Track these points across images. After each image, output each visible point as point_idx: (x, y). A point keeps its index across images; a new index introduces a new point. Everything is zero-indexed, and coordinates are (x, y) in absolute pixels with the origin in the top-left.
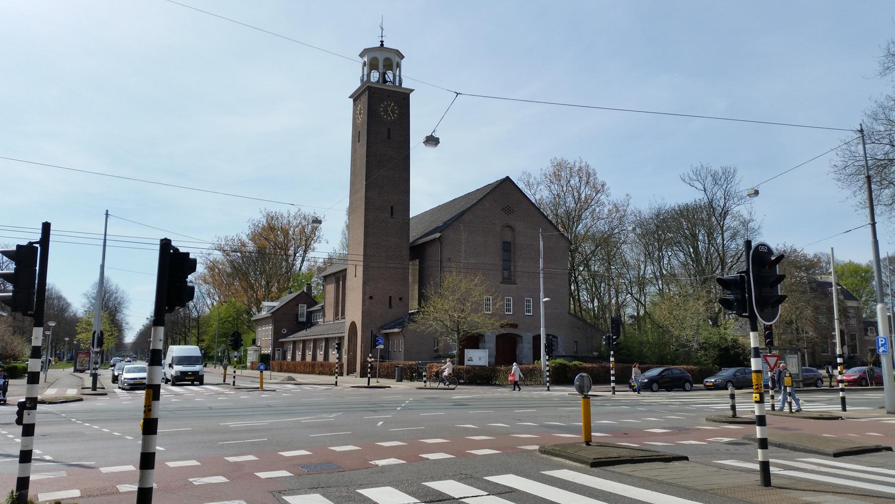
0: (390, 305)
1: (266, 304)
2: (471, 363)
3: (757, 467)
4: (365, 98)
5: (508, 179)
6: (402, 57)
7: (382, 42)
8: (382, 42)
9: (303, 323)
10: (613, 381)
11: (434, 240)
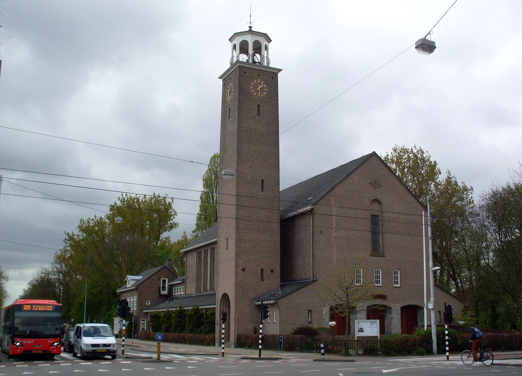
1: (130, 277)
6: (269, 40)
7: (250, 27)
8: (250, 27)
9: (164, 296)
10: (448, 351)
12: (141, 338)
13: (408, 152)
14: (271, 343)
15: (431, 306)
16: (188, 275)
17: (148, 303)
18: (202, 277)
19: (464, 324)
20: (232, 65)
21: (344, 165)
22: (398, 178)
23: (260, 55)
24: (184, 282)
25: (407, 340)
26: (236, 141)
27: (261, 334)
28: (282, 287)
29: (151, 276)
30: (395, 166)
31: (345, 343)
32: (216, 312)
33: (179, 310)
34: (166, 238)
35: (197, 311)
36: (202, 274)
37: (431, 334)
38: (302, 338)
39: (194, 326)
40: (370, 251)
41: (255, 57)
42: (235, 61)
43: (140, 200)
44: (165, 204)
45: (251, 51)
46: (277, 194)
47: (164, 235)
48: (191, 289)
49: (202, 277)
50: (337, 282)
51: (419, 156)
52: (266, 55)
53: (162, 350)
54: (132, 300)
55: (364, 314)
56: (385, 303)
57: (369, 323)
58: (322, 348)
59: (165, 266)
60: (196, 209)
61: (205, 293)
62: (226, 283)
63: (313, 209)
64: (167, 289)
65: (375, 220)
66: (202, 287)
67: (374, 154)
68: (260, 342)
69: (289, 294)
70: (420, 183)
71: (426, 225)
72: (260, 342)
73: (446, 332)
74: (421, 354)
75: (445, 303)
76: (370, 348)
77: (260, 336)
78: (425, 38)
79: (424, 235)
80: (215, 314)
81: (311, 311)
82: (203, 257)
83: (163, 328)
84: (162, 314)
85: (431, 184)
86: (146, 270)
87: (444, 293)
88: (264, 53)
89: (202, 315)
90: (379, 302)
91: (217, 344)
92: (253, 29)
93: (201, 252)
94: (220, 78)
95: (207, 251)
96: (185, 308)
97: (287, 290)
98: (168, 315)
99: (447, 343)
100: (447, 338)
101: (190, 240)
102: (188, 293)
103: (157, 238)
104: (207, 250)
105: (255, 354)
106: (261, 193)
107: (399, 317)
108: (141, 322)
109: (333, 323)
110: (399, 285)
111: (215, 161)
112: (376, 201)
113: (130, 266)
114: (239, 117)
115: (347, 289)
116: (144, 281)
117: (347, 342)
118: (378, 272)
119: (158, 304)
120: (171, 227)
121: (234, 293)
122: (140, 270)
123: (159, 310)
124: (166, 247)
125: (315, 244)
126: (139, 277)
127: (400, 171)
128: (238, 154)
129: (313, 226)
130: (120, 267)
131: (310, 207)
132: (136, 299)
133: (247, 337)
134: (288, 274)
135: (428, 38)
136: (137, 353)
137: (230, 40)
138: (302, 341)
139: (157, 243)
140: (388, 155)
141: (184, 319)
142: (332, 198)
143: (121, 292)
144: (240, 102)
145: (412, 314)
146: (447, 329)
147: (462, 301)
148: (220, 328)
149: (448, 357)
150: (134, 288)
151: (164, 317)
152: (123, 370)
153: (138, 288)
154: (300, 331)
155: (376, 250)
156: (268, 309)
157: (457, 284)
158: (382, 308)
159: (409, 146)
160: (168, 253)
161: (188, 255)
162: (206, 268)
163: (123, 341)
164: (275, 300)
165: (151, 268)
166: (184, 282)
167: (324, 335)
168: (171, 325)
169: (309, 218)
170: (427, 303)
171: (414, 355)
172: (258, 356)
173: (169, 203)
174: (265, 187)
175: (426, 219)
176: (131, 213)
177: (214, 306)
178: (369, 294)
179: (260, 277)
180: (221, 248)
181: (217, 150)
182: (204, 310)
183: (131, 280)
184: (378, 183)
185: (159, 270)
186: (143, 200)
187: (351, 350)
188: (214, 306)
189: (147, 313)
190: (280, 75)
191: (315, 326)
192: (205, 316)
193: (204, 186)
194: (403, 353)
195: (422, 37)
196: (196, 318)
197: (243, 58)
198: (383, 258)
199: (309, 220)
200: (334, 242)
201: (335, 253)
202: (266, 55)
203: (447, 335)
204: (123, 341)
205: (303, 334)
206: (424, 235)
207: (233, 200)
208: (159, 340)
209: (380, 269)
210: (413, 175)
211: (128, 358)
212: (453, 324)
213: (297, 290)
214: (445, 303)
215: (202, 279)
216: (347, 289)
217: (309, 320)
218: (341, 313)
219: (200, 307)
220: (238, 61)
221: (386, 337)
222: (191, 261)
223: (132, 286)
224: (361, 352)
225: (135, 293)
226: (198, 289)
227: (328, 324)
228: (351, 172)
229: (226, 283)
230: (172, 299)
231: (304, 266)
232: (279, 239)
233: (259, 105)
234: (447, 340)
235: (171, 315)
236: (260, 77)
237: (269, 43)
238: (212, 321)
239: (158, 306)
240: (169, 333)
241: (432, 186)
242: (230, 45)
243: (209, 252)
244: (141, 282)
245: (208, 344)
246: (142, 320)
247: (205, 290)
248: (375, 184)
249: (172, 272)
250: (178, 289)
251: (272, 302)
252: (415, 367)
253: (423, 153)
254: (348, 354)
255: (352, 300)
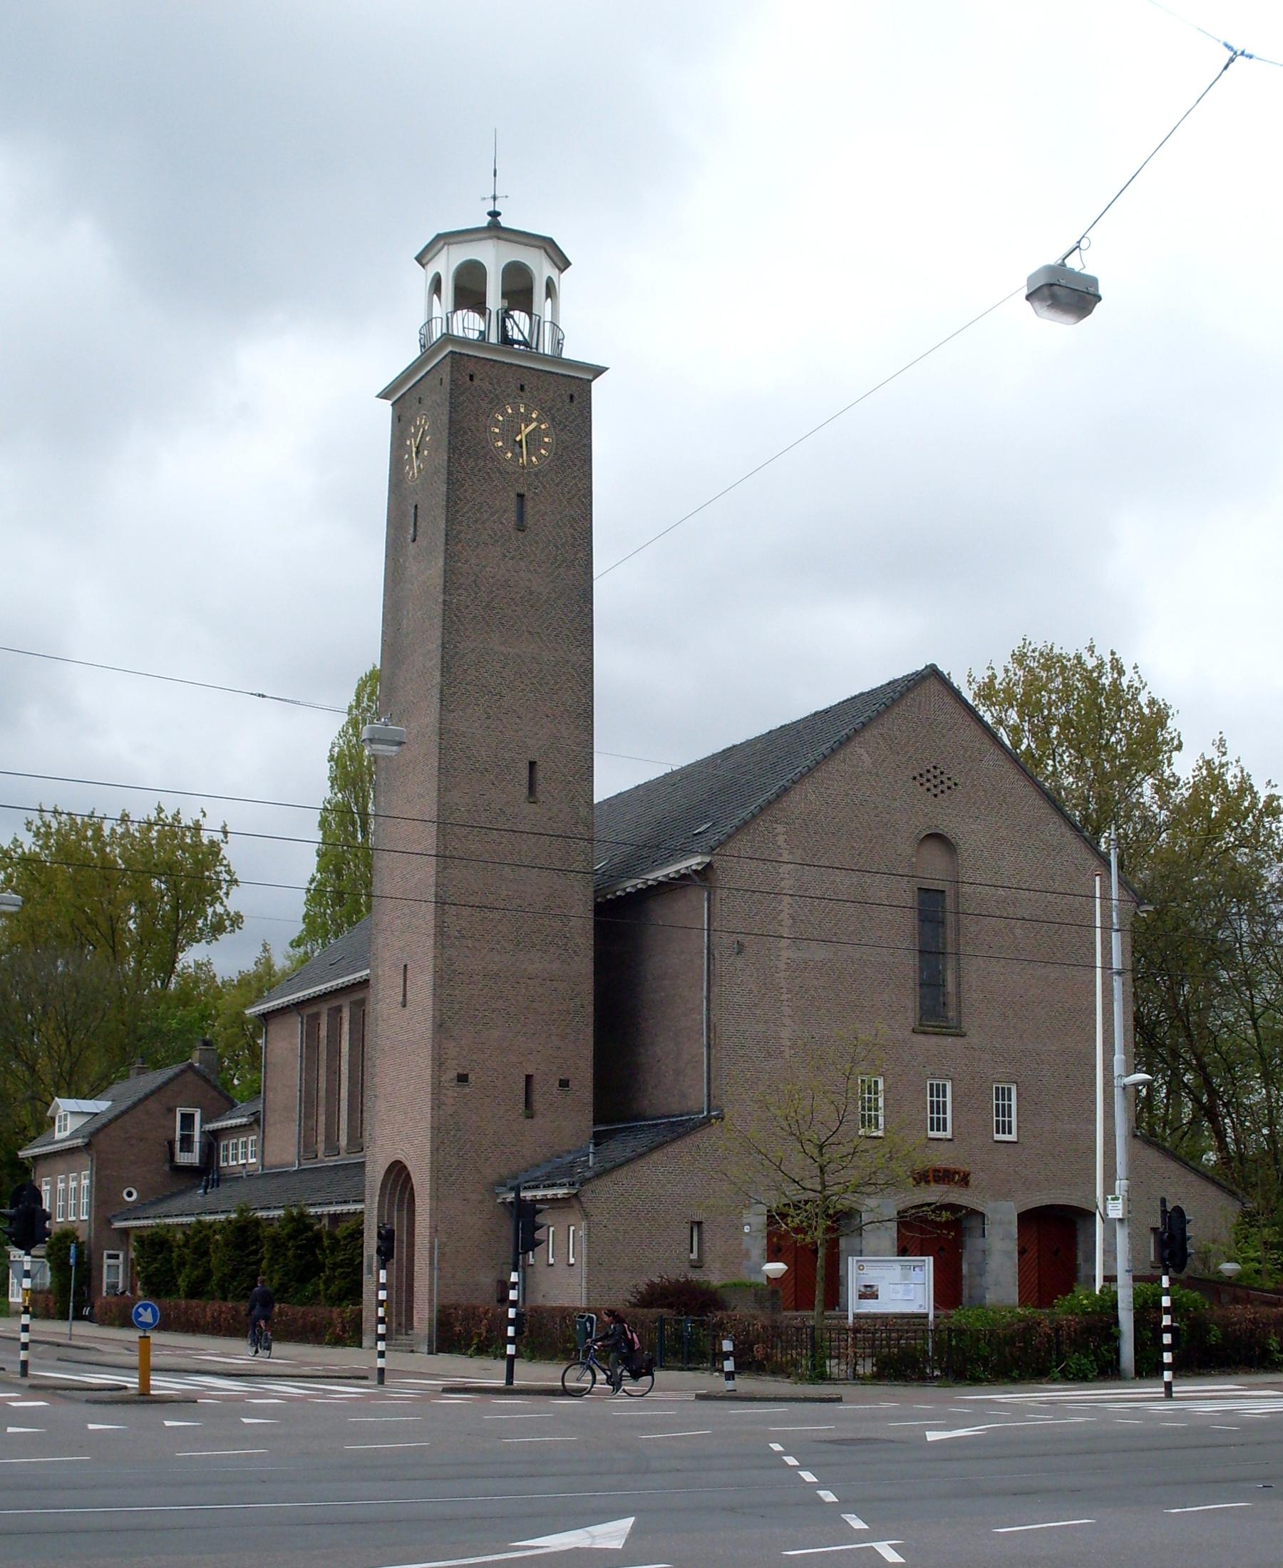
0: (528, 1104)
1: (64, 1105)
2: (870, 1307)
3: (31, 1372)
4: (438, 397)
5: (932, 677)
6: (562, 263)
7: (494, 214)
8: (494, 214)
10: (1169, 1367)
11: (684, 879)
12: (105, 1322)
13: (1064, 667)
14: (546, 1335)
15: (1116, 1210)
16: (270, 1095)
17: (130, 1194)
18: (323, 1102)
19: (1241, 1276)
20: (429, 350)
21: (826, 712)
22: (1011, 756)
23: (530, 314)
24: (257, 1122)
25: (1030, 1327)
26: (438, 622)
27: (514, 1304)
28: (598, 1139)
29: (141, 1101)
30: (1015, 716)
31: (812, 1338)
32: (365, 1226)
33: (237, 1221)
34: (199, 966)
35: (300, 1224)
36: (322, 1093)
37: (1115, 1306)
38: (662, 1321)
39: (282, 1277)
40: (910, 1017)
41: (509, 323)
42: (437, 335)
43: (106, 832)
44: (197, 844)
45: (494, 300)
46: (583, 812)
47: (189, 957)
48: (284, 1146)
49: (323, 1102)
50: (785, 1124)
51: (1106, 682)
52: (548, 317)
53: (154, 1360)
54: (73, 1184)
55: (889, 1235)
56: (955, 1196)
57: (897, 1267)
58: (726, 1356)
59: (191, 1066)
60: (303, 865)
61: (332, 1161)
62: (401, 1128)
63: (709, 865)
64: (197, 1146)
65: (932, 908)
66: (321, 1138)
67: (932, 673)
68: (511, 1331)
69: (621, 1165)
70: (1103, 778)
71: (1107, 929)
72: (511, 1331)
73: (1166, 1301)
74: (1080, 1377)
75: (1163, 1201)
76: (902, 1356)
77: (512, 1313)
78: (1063, 265)
79: (1099, 964)
80: (361, 1233)
81: (699, 1224)
82: (323, 1033)
83: (182, 1282)
84: (179, 1236)
85: (1140, 784)
86: (125, 1077)
87: (1173, 1165)
88: (543, 307)
89: (318, 1237)
90: (935, 1194)
91: (367, 1341)
92: (504, 221)
93: (316, 1016)
94: (384, 395)
95: (335, 1012)
96: (259, 1214)
97: (617, 1149)
98: (200, 1239)
99: (1167, 1339)
100: (1166, 1320)
101: (285, 974)
102: (271, 1159)
103: (168, 966)
104: (339, 1010)
105: (489, 1372)
106: (528, 809)
107: (1013, 1247)
108: (107, 1262)
109: (776, 1268)
110: (948, 1134)
111: (373, 693)
112: (937, 838)
113: (66, 1065)
114: (450, 537)
115: (821, 1147)
116: (117, 1118)
117: (817, 1333)
118: (939, 1091)
119: (173, 1195)
120: (218, 928)
121: (427, 1160)
122: (102, 1079)
123: (168, 1221)
124: (200, 994)
125: (715, 989)
126: (99, 1105)
127: (1034, 734)
128: (445, 669)
129: (709, 930)
130: (32, 1069)
131: (699, 859)
132: (85, 1182)
133: (471, 1315)
134: (621, 1099)
135: (1073, 263)
136: (76, 1373)
137: (421, 259)
138: (662, 1329)
139: (165, 985)
140: (993, 678)
141: (256, 1252)
142: (780, 829)
143: (35, 1158)
144: (451, 481)
145: (1056, 1235)
146: (1167, 1292)
147: (1233, 1194)
148: (376, 1283)
149: (1168, 1386)
150: (79, 1142)
151: (186, 1245)
152: (10, 1430)
153: (94, 1141)
154: (656, 1296)
155: (936, 1010)
156: (539, 1219)
157: (1220, 1134)
158: (946, 1216)
159: (1068, 646)
160: (204, 1017)
161: (275, 1028)
162: (334, 1071)
163: (25, 1328)
164: (572, 1185)
165: (141, 1071)
166: (257, 1121)
167: (743, 1309)
168: (208, 1273)
169: (697, 900)
170: (1105, 1200)
171: (1054, 1381)
172: (501, 1383)
173: (212, 842)
174: (541, 786)
175: (1106, 900)
176: (73, 879)
177: (359, 1207)
178: (901, 1170)
179: (522, 1106)
180: (384, 1002)
181: (370, 655)
182: (325, 1221)
183: (71, 1115)
184: (944, 778)
185: (171, 1080)
186: (119, 830)
187: (834, 1362)
188: (359, 1207)
189: (125, 1232)
190: (599, 388)
191: (714, 1277)
192: (326, 1242)
193: (333, 780)
194: (1015, 1374)
195: (1053, 260)
196: (298, 1247)
197: (469, 324)
198: (962, 1040)
199: (694, 907)
200: (783, 984)
201: (787, 1021)
202: (548, 317)
203: (1167, 1311)
204: (25, 1328)
205: (670, 1306)
206: (1099, 964)
207: (427, 839)
208: (145, 1326)
209: (947, 1077)
210: (1078, 751)
211: (39, 1389)
212: (1188, 1271)
213: (651, 1150)
214: (1163, 1201)
215: (322, 1110)
216: (821, 1147)
217: (694, 1256)
218: (798, 1230)
219: (312, 1211)
220: (448, 338)
221: (957, 1317)
222: (284, 1047)
223: (73, 1136)
224: (866, 1368)
225: (86, 1159)
226: (307, 1146)
227: (760, 1272)
228: (849, 738)
229: (401, 1128)
230: (217, 1183)
231: (677, 1066)
232: (591, 967)
233: (521, 496)
234: (1168, 1329)
235: (207, 1238)
236: (527, 394)
237: (562, 271)
238: (352, 1260)
239: (164, 1208)
240: (202, 1303)
241: (1147, 789)
242: (422, 278)
243: (346, 1014)
244: (104, 1120)
245: (338, 1341)
246: (110, 1257)
247: (332, 1148)
248: (934, 781)
249: (215, 1087)
250: (236, 1146)
251: (561, 1192)
252: (1046, 1420)
253: (1121, 672)
254: (821, 1376)
255: (836, 1188)
